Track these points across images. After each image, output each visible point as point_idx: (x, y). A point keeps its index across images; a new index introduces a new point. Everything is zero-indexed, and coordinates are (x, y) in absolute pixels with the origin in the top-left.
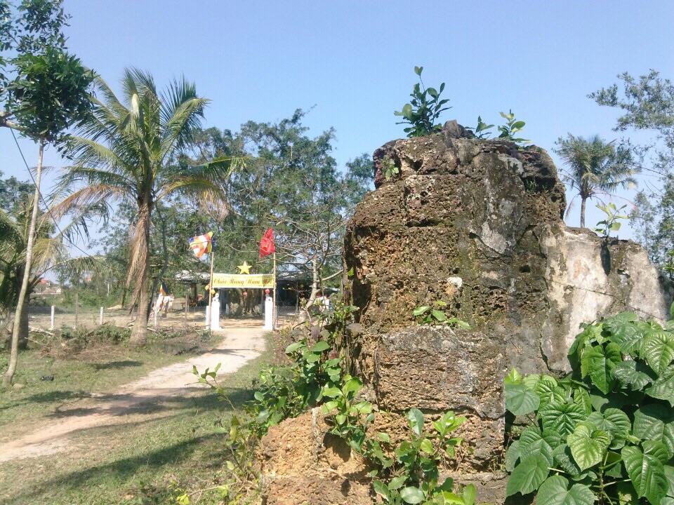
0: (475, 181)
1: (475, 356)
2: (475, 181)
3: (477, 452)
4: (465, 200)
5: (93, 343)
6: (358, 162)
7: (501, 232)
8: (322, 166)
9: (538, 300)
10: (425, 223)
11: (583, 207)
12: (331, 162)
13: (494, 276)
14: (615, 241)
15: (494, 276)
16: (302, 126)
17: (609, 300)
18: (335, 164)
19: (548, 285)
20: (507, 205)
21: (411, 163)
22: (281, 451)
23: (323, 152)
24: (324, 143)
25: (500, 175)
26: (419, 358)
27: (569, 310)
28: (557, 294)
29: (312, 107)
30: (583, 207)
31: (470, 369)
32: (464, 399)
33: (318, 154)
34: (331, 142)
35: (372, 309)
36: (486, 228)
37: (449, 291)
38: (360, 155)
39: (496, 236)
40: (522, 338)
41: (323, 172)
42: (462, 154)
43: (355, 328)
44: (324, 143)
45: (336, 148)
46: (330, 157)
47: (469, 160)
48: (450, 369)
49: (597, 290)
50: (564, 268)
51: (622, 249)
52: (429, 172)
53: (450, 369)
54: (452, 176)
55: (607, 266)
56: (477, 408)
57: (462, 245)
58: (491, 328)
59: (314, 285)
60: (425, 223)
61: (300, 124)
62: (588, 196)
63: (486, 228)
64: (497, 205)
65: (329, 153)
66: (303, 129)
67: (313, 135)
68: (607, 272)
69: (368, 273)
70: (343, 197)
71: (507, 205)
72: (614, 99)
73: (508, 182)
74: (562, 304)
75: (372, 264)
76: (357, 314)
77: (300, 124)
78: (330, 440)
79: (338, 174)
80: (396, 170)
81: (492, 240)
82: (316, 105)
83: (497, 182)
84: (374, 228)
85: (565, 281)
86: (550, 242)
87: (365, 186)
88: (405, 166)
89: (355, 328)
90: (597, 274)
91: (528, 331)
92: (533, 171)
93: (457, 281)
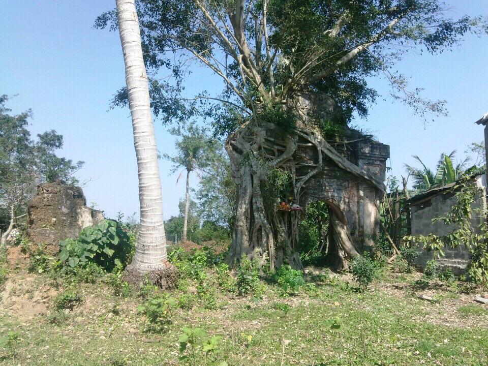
0: (61, 196)
1: (54, 234)
2: (61, 196)
3: (53, 252)
4: (58, 201)
5: (234, 173)
6: (46, 135)
7: (67, 208)
8: (18, 136)
9: (75, 224)
10: (48, 206)
11: (188, 177)
12: (26, 133)
13: (65, 218)
14: (95, 211)
15: (65, 218)
16: (6, 107)
17: (92, 224)
18: (30, 135)
19: (78, 220)
20: (69, 202)
21: (46, 190)
22: (11, 253)
23: (21, 126)
24: (22, 119)
25: (67, 195)
26: (42, 234)
27: (82, 226)
28: (80, 223)
29: (15, 95)
30: (188, 177)
31: (53, 237)
32: (51, 242)
33: (17, 127)
34: (28, 119)
35: (33, 225)
36: (63, 207)
37: (52, 222)
38: (49, 131)
39: (65, 209)
40: (71, 232)
41: (19, 140)
42: (58, 190)
43: (29, 230)
44: (22, 119)
45: (31, 124)
46: (26, 130)
47: (60, 191)
48: (48, 237)
49: (90, 222)
50: (82, 216)
51: (96, 212)
52: (50, 193)
53: (48, 237)
54: (55, 195)
55: (92, 216)
56: (54, 244)
57: (57, 211)
58: (63, 230)
59: (12, 221)
60: (48, 206)
61: (3, 105)
62: (191, 170)
63: (63, 207)
64: (66, 202)
65: (25, 127)
66: (7, 110)
67: (14, 113)
68: (92, 217)
69: (33, 217)
70: (34, 159)
71: (69, 202)
72: (179, 132)
73: (69, 197)
74: (81, 225)
75: (34, 215)
76: (30, 227)
77: (3, 105)
78: (22, 251)
79: (31, 142)
80: (42, 192)
81: (65, 210)
82: (18, 94)
83: (66, 196)
84: (35, 206)
85: (82, 220)
86: (79, 211)
87: (51, 152)
88: (44, 191)
89: (29, 230)
90: (90, 218)
91: (72, 231)
92: (76, 193)
93: (55, 219)
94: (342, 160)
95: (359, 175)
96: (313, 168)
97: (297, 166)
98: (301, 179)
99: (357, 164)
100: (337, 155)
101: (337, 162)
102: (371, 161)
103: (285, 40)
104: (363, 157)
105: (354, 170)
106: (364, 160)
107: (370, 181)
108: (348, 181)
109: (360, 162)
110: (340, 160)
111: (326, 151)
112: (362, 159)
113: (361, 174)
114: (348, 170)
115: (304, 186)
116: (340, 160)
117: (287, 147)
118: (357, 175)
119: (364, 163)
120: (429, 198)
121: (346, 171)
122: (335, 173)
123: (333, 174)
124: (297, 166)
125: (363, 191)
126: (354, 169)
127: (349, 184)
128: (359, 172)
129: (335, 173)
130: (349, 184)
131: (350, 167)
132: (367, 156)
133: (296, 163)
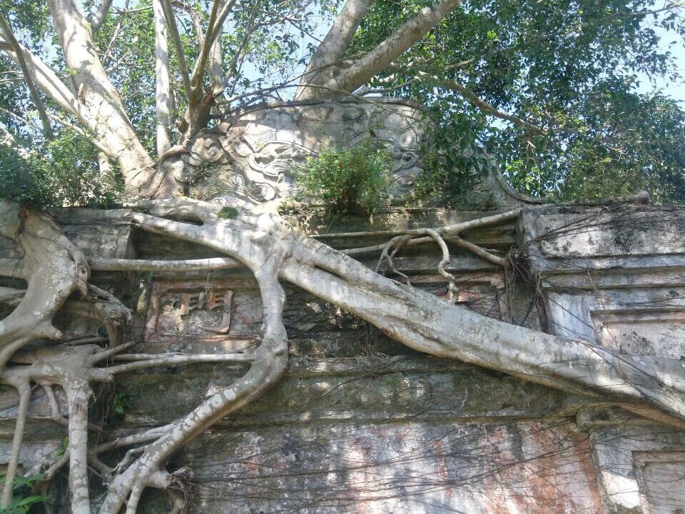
94: (412, 306)
95: (555, 375)
96: (229, 371)
97: (105, 374)
98: (150, 441)
99: (547, 326)
100: (373, 288)
101: (382, 324)
102: (642, 298)
103: (547, 31)
104: (575, 281)
105: (505, 351)
106: (589, 299)
107: (647, 402)
108: (511, 423)
109: (562, 310)
110: (398, 309)
111: (306, 279)
112: (572, 291)
113: (570, 370)
114: (470, 356)
115: (161, 479)
116: (398, 309)
117: (31, 284)
118: (547, 381)
119: (594, 315)
120: (596, 254)
121: (459, 362)
122: (395, 385)
123: (386, 393)
124: (105, 374)
125: (632, 475)
126: (507, 344)
127: (518, 442)
128: (546, 361)
129: (395, 385)
130: (518, 442)
131: (475, 338)
132: (592, 272)
133: (102, 354)
